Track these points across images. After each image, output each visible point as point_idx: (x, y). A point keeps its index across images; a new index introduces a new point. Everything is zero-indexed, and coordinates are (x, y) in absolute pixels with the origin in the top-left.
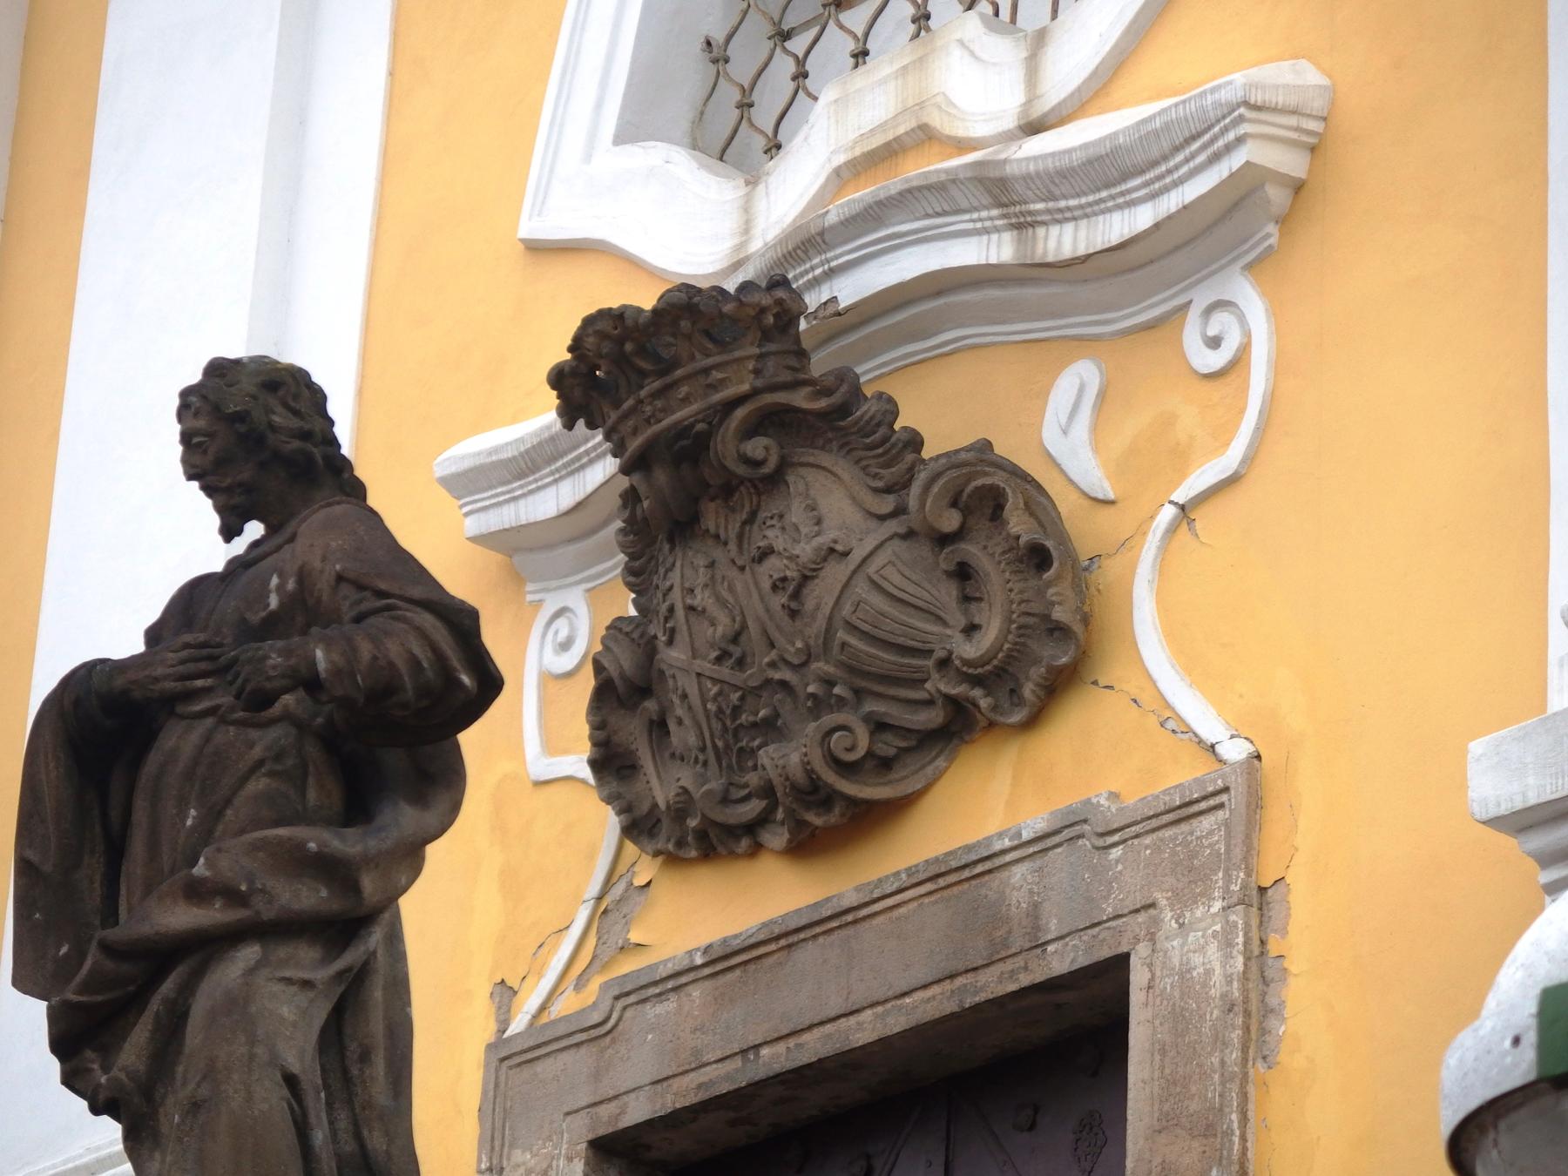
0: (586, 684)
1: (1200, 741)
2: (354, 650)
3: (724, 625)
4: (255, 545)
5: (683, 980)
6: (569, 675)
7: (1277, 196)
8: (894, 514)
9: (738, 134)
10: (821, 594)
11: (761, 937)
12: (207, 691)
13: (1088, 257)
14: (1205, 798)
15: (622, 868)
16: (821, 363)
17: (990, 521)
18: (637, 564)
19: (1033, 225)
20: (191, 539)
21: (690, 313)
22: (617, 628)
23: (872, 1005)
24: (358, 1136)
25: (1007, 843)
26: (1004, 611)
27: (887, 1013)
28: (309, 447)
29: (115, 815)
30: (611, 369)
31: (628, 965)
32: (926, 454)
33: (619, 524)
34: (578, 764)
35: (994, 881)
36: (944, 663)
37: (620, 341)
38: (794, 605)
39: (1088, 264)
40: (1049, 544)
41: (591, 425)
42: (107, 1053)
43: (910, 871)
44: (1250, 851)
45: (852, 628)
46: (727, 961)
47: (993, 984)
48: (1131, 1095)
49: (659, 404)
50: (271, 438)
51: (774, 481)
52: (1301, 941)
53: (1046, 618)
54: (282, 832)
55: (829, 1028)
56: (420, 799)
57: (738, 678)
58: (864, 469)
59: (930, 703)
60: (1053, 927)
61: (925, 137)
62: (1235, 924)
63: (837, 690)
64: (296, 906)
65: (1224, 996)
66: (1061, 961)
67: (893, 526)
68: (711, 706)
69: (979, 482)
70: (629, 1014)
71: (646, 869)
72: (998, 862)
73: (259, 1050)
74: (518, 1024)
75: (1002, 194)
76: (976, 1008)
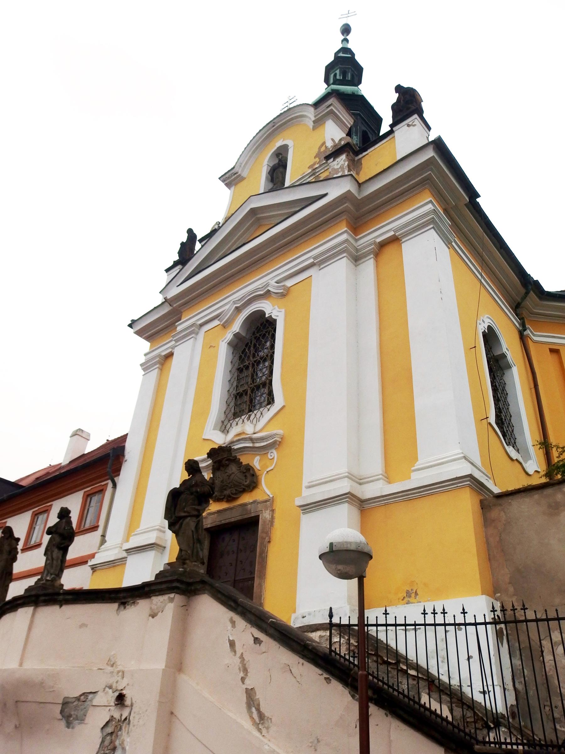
7: (278, 443)
9: (224, 429)
16: (233, 455)
21: (221, 449)
30: (213, 453)
44: (272, 506)
46: (219, 512)
47: (246, 517)
51: (228, 466)
52: (276, 515)
61: (244, 433)
66: (253, 515)
75: (251, 440)
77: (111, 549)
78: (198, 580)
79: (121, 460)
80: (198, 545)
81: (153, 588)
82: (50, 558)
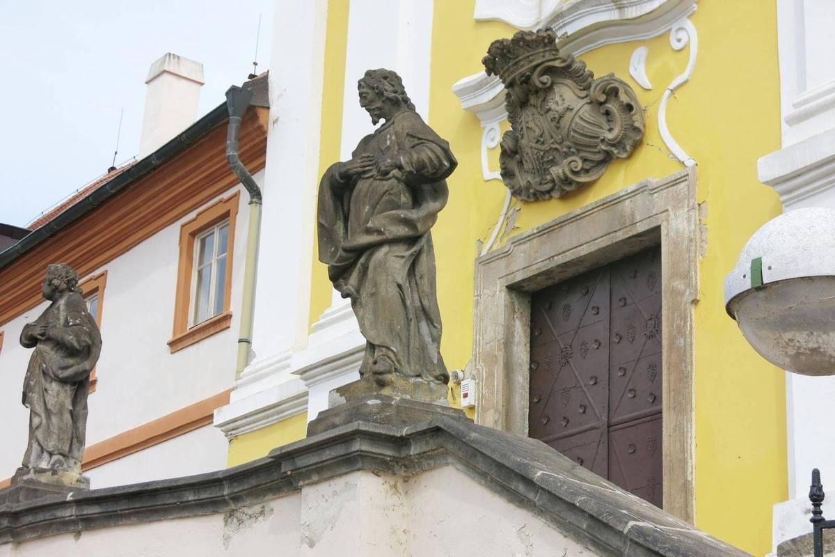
0: (499, 151)
1: (680, 161)
2: (412, 156)
3: (538, 132)
4: (383, 125)
5: (531, 237)
6: (494, 148)
8: (586, 97)
10: (565, 122)
11: (553, 224)
12: (370, 170)
13: (641, 16)
14: (681, 178)
15: (512, 205)
17: (611, 97)
18: (512, 115)
19: (623, 7)
20: (358, 125)
21: (522, 40)
22: (506, 134)
23: (586, 243)
24: (420, 301)
25: (624, 193)
26: (619, 125)
27: (590, 246)
28: (397, 95)
29: (346, 208)
31: (515, 234)
32: (595, 78)
33: (506, 103)
34: (497, 174)
35: (620, 206)
36: (603, 141)
37: (502, 49)
38: (558, 125)
39: (640, 19)
40: (632, 103)
41: (496, 74)
42: (346, 279)
43: (596, 203)
45: (575, 131)
47: (621, 236)
48: (663, 267)
49: (515, 67)
50: (385, 93)
51: (551, 88)
53: (632, 125)
54: (393, 212)
55: (574, 250)
56: (435, 199)
57: (543, 147)
58: (577, 83)
59: (599, 152)
60: (638, 218)
62: (691, 215)
63: (572, 150)
64: (398, 234)
65: (689, 237)
66: (641, 228)
67: (587, 100)
68: (535, 157)
69: (611, 86)
70: (515, 249)
71: (519, 205)
72: (621, 199)
73: (389, 277)
74: (484, 253)
76: (617, 243)
77: (266, 375)
78: (423, 426)
79: (262, 121)
80: (424, 325)
81: (302, 462)
82: (39, 409)
